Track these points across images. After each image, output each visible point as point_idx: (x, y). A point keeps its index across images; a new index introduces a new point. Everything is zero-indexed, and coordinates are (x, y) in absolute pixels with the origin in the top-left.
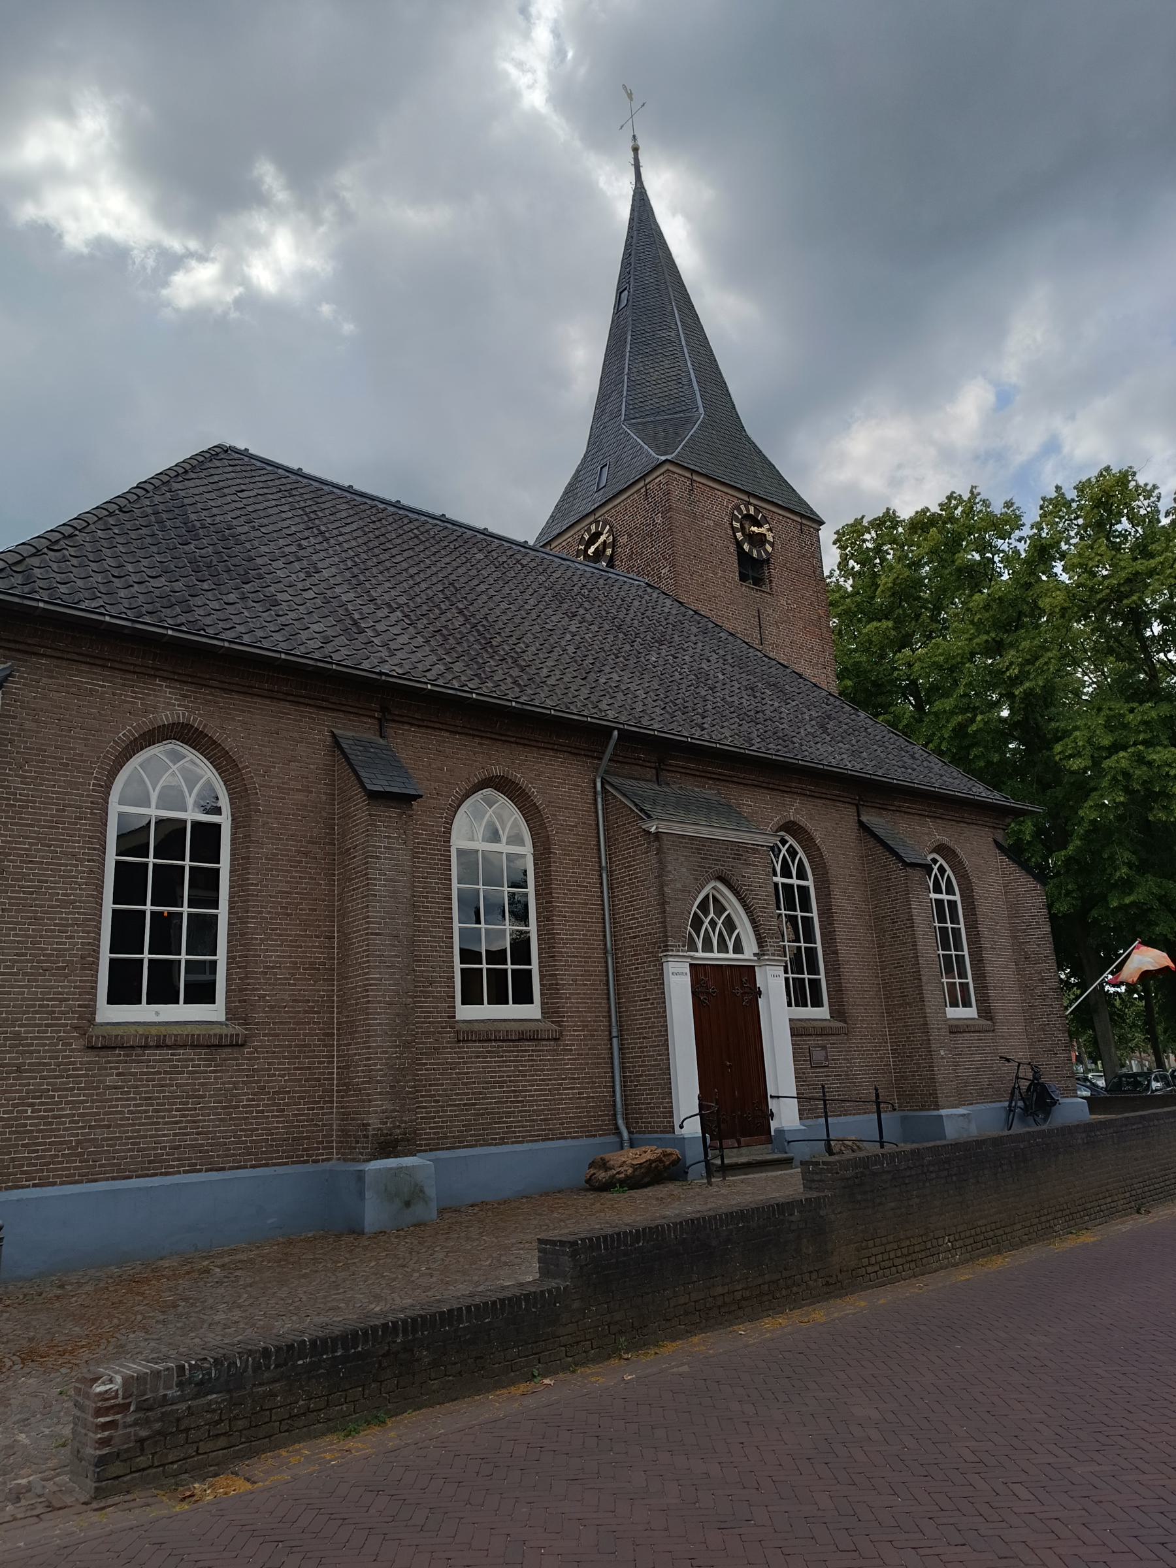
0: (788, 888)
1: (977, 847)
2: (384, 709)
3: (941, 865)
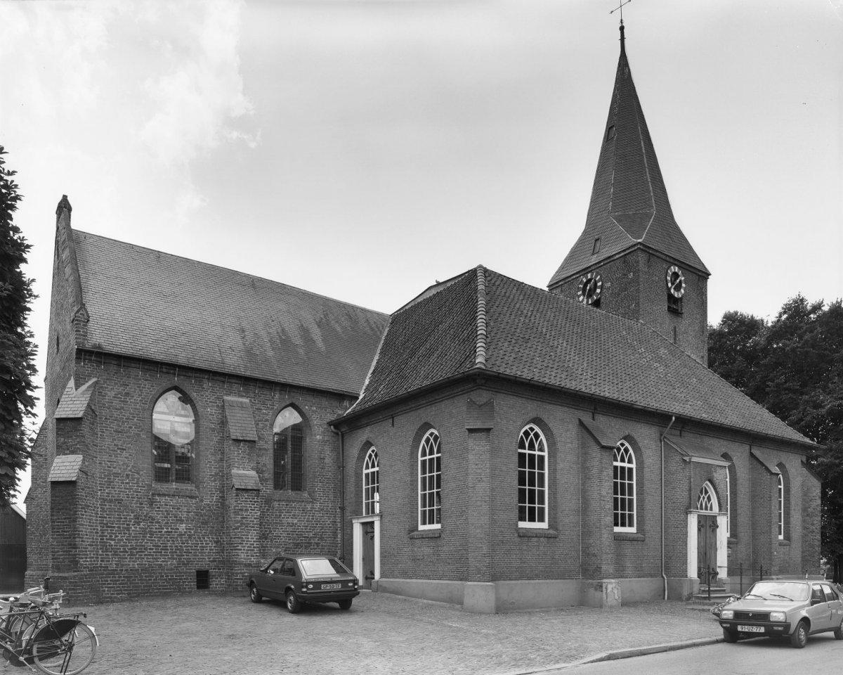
0: (623, 468)
1: (794, 463)
2: (595, 409)
3: (536, 433)
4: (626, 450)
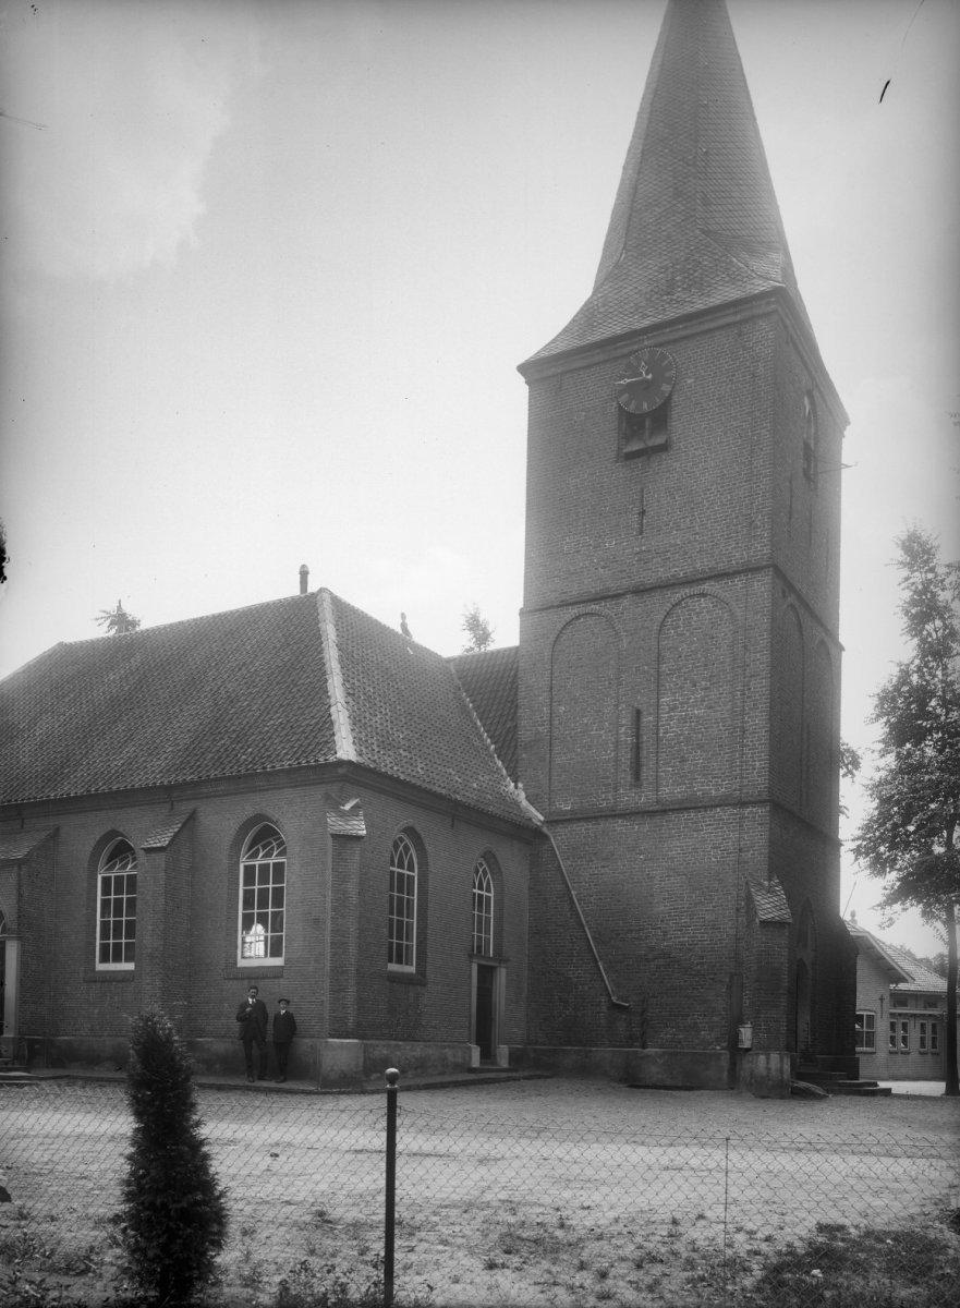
0: (480, 896)
4: (406, 848)
